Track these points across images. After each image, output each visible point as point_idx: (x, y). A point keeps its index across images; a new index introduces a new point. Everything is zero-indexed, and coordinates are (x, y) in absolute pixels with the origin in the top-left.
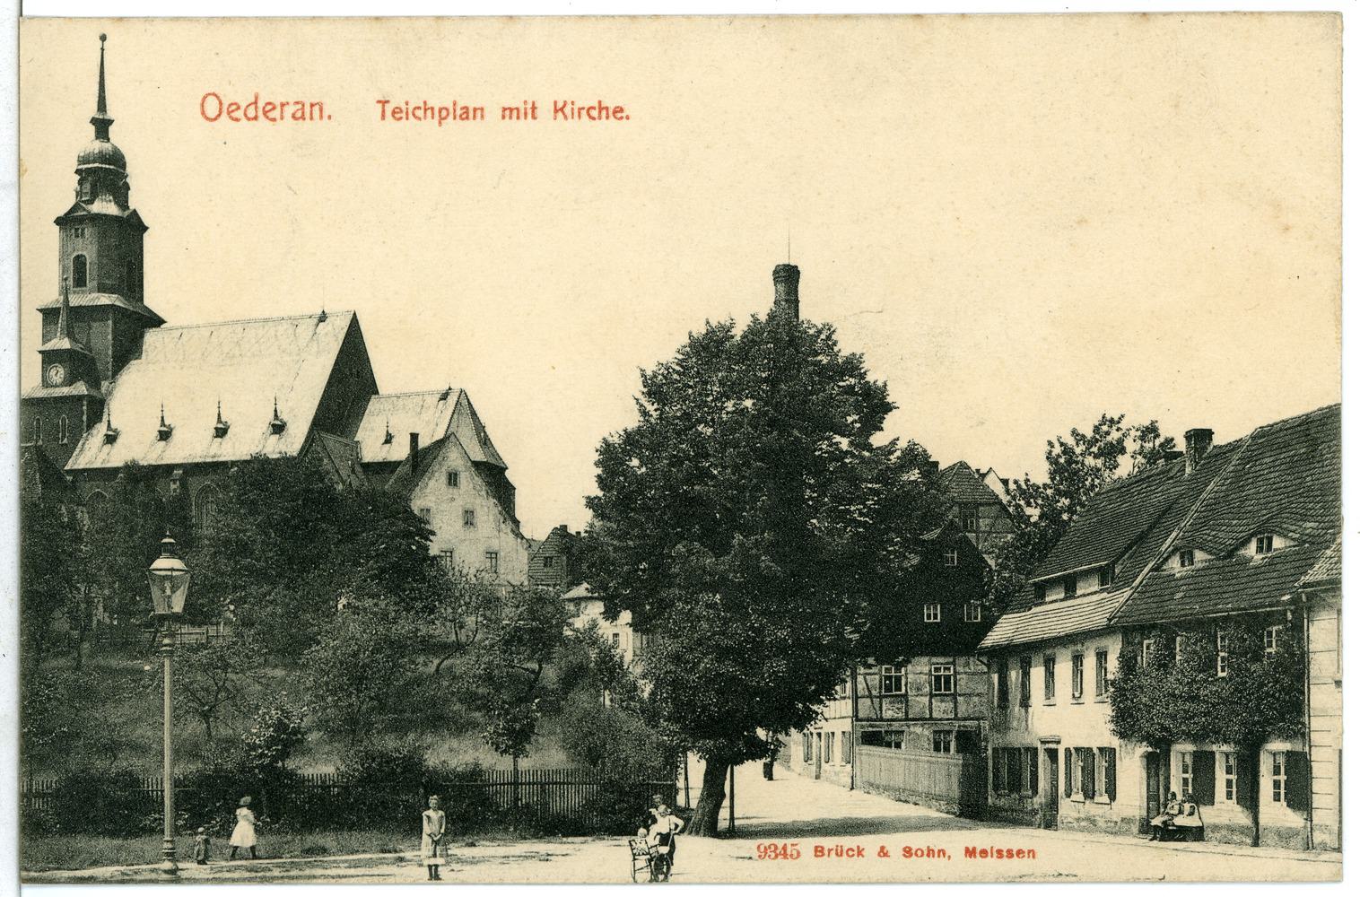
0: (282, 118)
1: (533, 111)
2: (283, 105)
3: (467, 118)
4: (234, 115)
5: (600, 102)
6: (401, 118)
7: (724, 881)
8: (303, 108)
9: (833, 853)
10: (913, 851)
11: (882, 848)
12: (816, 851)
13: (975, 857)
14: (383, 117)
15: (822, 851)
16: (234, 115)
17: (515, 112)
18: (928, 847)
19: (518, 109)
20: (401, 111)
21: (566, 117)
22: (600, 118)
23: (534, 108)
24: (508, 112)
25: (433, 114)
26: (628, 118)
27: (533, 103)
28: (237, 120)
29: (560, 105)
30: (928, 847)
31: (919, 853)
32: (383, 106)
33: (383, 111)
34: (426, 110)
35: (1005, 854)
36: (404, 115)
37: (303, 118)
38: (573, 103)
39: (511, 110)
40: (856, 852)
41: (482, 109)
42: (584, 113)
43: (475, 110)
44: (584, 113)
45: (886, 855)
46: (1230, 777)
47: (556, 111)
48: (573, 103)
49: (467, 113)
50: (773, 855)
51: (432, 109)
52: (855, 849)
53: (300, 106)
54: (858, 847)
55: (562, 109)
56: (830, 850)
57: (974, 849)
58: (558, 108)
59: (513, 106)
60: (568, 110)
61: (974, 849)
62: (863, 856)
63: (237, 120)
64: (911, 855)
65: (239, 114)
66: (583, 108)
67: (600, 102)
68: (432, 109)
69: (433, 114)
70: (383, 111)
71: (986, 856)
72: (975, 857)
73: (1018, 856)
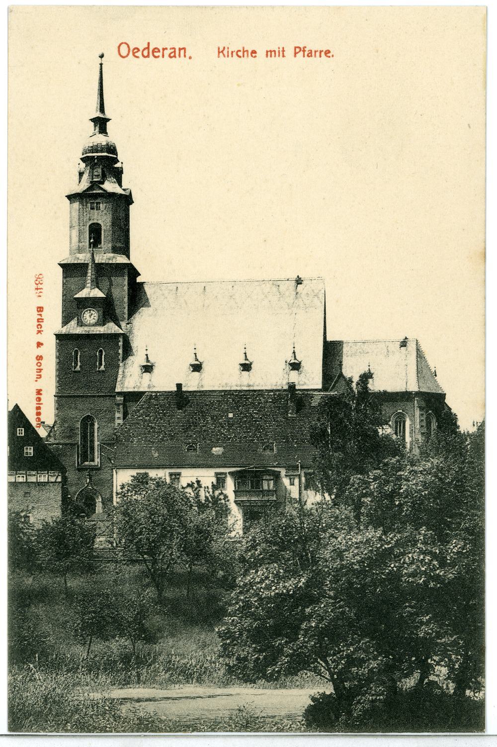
0: (163, 56)
1: (283, 53)
2: (164, 49)
3: (311, 56)
4: (136, 54)
5: (244, 48)
6: (159, 57)
7: (9, 26)
8: (175, 52)
9: (39, 317)
10: (40, 361)
11: (42, 344)
12: (40, 307)
13: (37, 395)
14: (304, 56)
15: (40, 311)
16: (136, 54)
17: (273, 53)
18: (42, 369)
19: (275, 51)
20: (159, 51)
21: (224, 56)
22: (243, 56)
23: (283, 51)
24: (270, 53)
25: (275, 54)
26: (333, 56)
27: (283, 48)
28: (137, 57)
29: (221, 49)
30: (42, 369)
31: (39, 364)
32: (223, 53)
33: (304, 54)
34: (244, 52)
35: (39, 411)
36: (160, 54)
37: (175, 56)
38: (228, 48)
39: (271, 51)
40: (40, 329)
41: (184, 49)
42: (234, 54)
43: (180, 49)
44: (323, 54)
45: (42, 344)
46: (40, 385)
47: (219, 52)
48: (228, 48)
49: (311, 53)
50: (37, 282)
51: (247, 51)
52: (42, 329)
53: (173, 50)
54: (43, 331)
55: (222, 52)
56: (41, 315)
57: (41, 394)
58: (220, 51)
59: (272, 50)
60: (225, 52)
61: (41, 394)
62: (37, 334)
63: (137, 57)
64: (38, 360)
65: (139, 54)
66: (166, 49)
67: (244, 48)
68: (247, 51)
69: (275, 54)
70: (304, 54)
71: (37, 401)
72: (37, 395)
73: (37, 418)
